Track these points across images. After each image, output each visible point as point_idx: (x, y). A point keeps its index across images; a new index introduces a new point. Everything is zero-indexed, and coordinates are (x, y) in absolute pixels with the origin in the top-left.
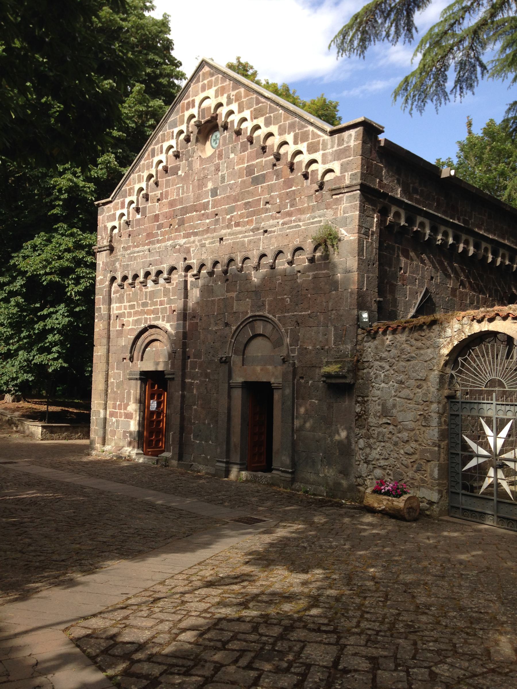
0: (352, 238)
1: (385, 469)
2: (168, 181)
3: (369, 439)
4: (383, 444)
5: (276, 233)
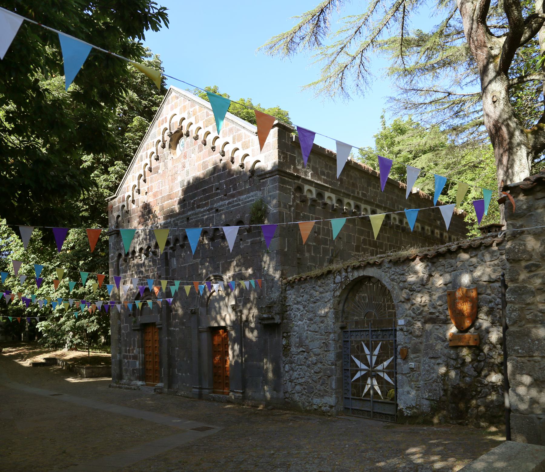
0: (275, 211)
1: (302, 385)
2: (152, 178)
3: (291, 364)
4: (301, 367)
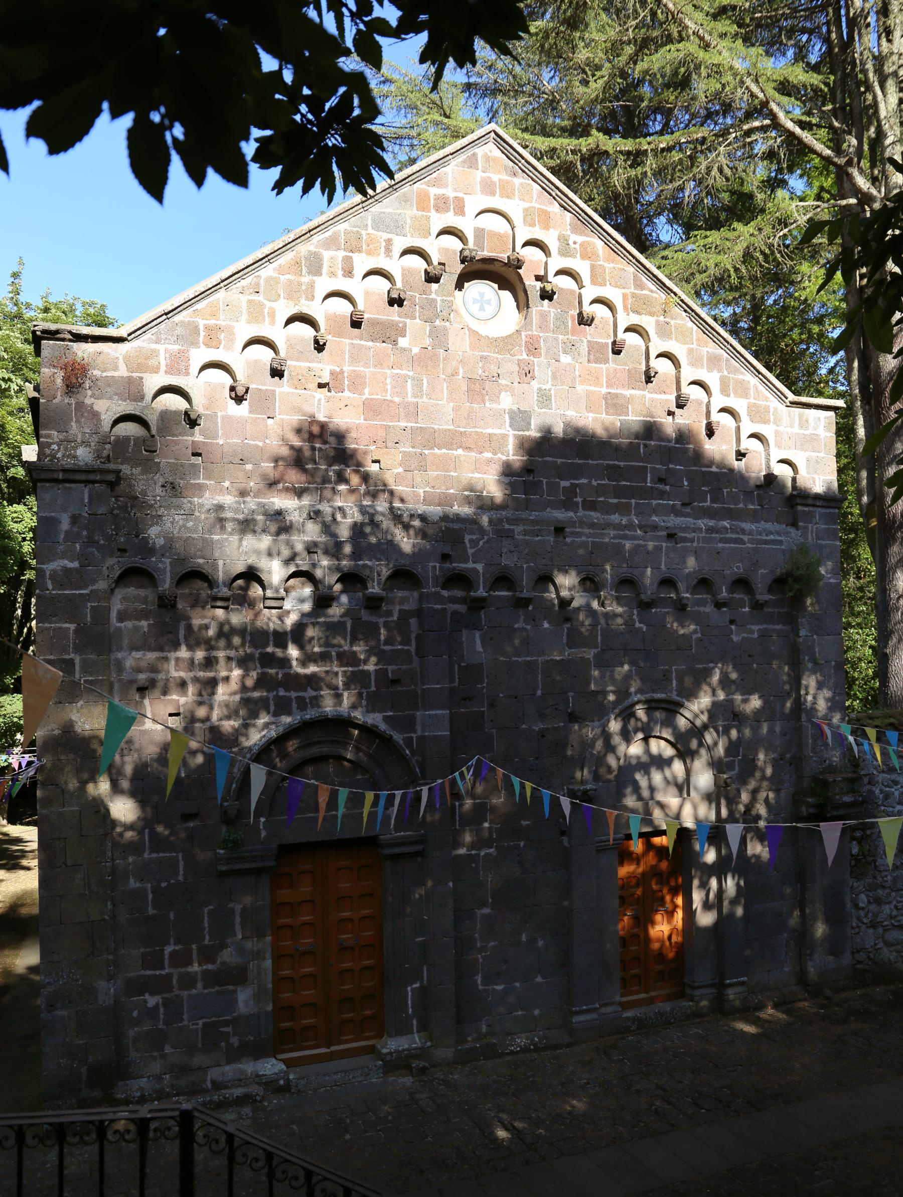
0: (832, 580)
5: (695, 544)
